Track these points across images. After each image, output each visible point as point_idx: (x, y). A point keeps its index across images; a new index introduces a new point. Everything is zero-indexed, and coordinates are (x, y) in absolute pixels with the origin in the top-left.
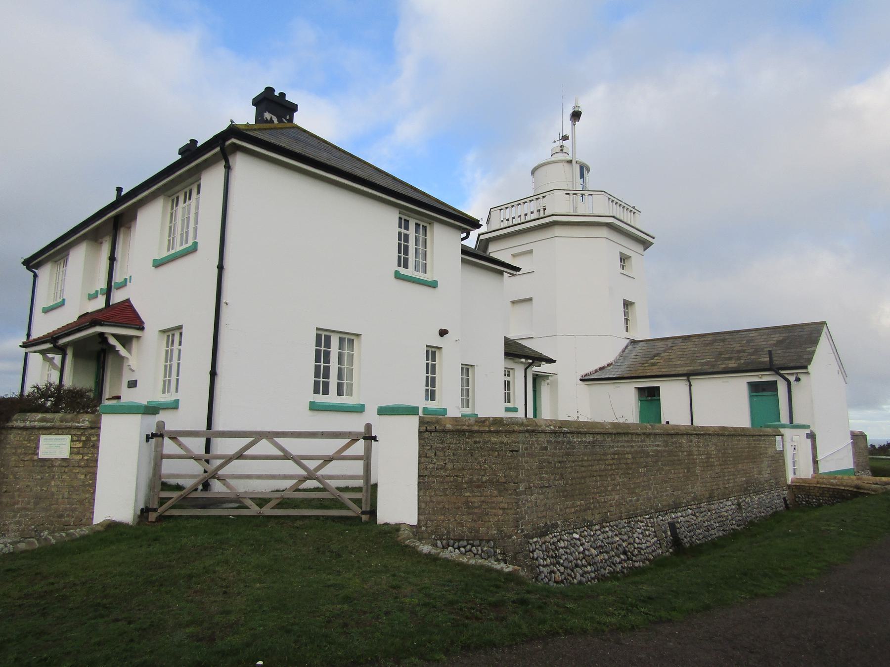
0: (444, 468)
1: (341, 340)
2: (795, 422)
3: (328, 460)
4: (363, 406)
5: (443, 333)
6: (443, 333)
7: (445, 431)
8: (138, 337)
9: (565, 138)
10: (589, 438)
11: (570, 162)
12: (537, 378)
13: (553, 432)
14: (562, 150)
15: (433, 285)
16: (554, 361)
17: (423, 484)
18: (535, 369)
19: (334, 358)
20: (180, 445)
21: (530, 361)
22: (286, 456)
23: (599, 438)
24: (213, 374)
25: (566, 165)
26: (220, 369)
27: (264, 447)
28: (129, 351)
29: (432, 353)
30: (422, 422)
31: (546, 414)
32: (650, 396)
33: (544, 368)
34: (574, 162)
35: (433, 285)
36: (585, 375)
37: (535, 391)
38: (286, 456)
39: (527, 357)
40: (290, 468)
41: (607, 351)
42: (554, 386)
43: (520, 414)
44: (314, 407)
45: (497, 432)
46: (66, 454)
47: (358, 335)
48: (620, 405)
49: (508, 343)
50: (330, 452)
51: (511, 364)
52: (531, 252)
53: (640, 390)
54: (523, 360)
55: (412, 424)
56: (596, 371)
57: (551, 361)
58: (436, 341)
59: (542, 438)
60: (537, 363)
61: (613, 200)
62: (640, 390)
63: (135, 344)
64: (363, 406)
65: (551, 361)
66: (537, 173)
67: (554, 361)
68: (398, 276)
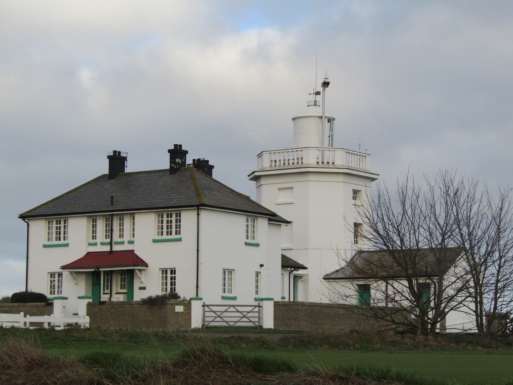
0: (280, 314)
1: (229, 272)
2: (199, 296)
3: (249, 312)
4: (236, 297)
5: (262, 266)
6: (262, 266)
7: (280, 305)
8: (144, 270)
9: (318, 93)
10: (319, 308)
11: (321, 117)
12: (296, 278)
13: (309, 306)
14: (315, 104)
15: (257, 245)
16: (307, 268)
17: (275, 319)
18: (294, 272)
19: (62, 233)
20: (209, 308)
21: (293, 269)
22: (238, 311)
23: (322, 308)
24: (197, 287)
25: (318, 119)
26: (199, 285)
27: (232, 309)
28: (141, 274)
29: (257, 274)
30: (275, 302)
31: (300, 299)
32: (364, 290)
33: (301, 272)
34: (323, 117)
35: (257, 245)
36: (326, 276)
37: (294, 286)
38: (238, 311)
39: (291, 267)
40: (239, 315)
41: (335, 264)
42: (306, 282)
43: (287, 300)
44: (223, 298)
45: (294, 305)
46: (183, 311)
47: (233, 270)
48: (347, 293)
49: (284, 258)
50: (249, 310)
51: (284, 272)
52: (292, 188)
53: (359, 285)
54: (289, 269)
55: (271, 303)
56: (333, 273)
57: (305, 268)
58: (259, 269)
59: (306, 307)
60: (296, 269)
61: (348, 152)
62: (359, 285)
63: (143, 272)
64: (236, 297)
65: (305, 268)
66: (296, 120)
67: (307, 268)
68: (246, 244)
